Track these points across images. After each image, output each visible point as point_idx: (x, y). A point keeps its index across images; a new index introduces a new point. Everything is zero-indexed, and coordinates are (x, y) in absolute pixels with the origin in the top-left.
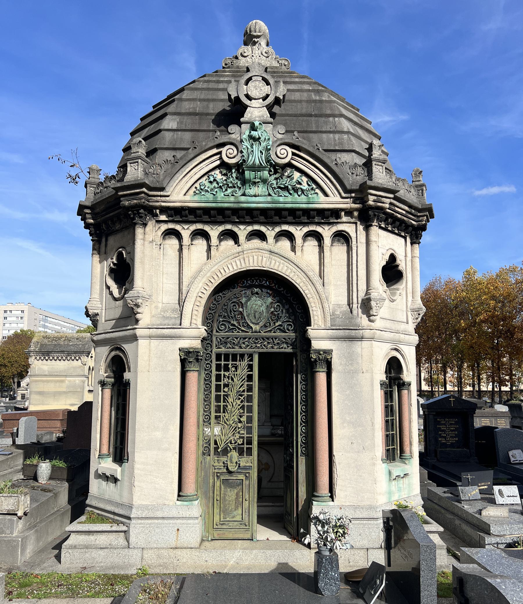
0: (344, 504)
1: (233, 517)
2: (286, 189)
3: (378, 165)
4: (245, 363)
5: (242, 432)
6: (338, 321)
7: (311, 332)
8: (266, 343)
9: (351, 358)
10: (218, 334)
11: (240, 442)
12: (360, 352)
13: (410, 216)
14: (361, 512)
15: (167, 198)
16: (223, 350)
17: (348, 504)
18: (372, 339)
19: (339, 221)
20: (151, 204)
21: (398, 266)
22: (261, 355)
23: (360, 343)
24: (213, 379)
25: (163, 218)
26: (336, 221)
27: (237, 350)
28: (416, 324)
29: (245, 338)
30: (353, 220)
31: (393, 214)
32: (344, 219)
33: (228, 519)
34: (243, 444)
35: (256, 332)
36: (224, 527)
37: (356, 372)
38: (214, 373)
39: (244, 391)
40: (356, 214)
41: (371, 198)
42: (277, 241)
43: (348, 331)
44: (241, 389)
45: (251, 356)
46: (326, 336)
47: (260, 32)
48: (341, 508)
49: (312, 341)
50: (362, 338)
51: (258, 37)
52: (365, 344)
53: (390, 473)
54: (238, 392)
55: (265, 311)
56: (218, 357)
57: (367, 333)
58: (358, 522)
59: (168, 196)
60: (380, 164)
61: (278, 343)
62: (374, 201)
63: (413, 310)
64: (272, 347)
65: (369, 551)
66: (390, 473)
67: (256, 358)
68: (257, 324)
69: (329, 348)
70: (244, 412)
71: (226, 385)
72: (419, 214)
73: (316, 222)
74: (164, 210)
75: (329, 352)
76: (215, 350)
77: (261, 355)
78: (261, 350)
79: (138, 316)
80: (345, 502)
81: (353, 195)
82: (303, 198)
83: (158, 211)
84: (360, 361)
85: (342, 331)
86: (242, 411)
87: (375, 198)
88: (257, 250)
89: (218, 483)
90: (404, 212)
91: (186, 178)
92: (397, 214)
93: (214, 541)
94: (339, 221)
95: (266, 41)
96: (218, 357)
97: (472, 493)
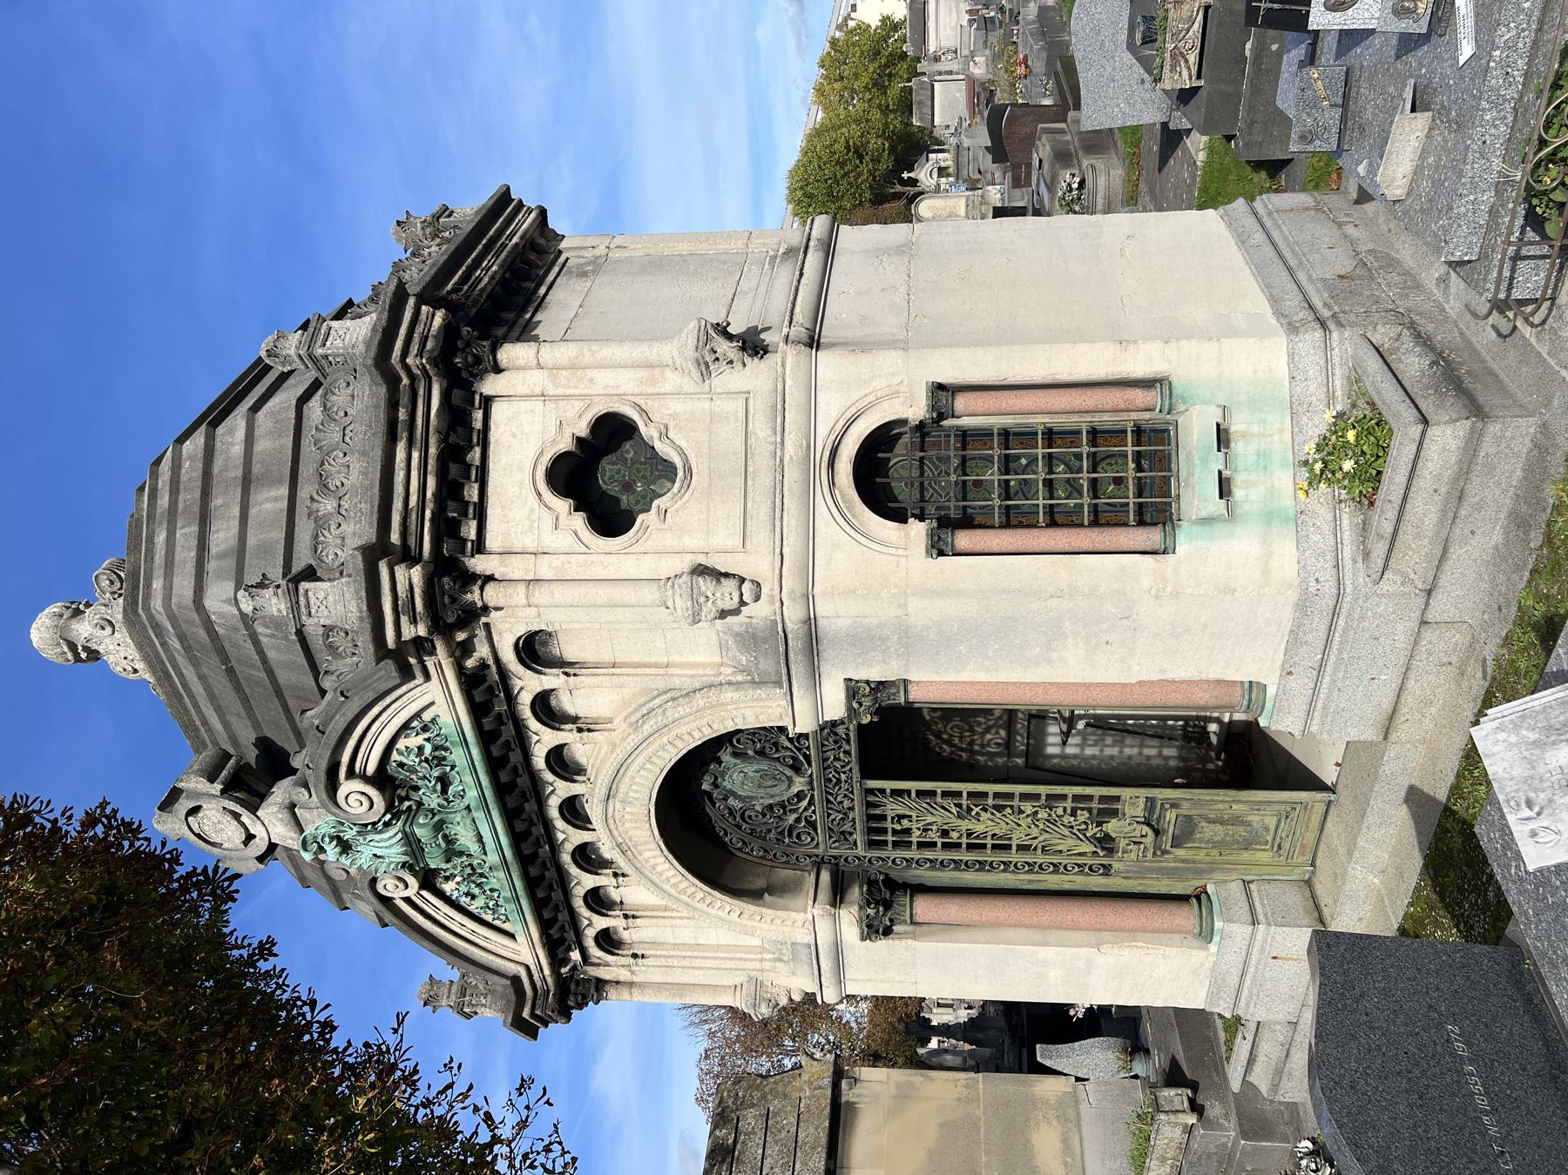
0: (1279, 663)
1: (1268, 830)
2: (444, 781)
3: (308, 605)
4: (892, 808)
5: (1060, 811)
6: (768, 665)
7: (805, 724)
8: (837, 764)
9: (864, 640)
10: (822, 846)
11: (1083, 816)
12: (849, 622)
13: (419, 421)
14: (1311, 631)
15: (533, 967)
16: (859, 837)
17: (1280, 656)
18: (808, 598)
19: (491, 662)
20: (552, 988)
21: (580, 441)
22: (865, 774)
23: (821, 622)
24: (929, 854)
25: (575, 955)
26: (494, 668)
27: (857, 814)
28: (748, 360)
29: (828, 801)
30: (481, 633)
31: (432, 520)
32: (482, 651)
33: (1269, 838)
34: (1090, 810)
35: (811, 782)
36: (1286, 845)
37: (906, 632)
38: (913, 854)
39: (959, 806)
40: (461, 636)
41: (408, 632)
42: (581, 770)
43: (791, 655)
44: (954, 810)
45: (870, 791)
46: (811, 698)
47: (59, 644)
48: (1290, 673)
49: (827, 718)
50: (810, 623)
51: (72, 646)
52: (823, 608)
53: (1207, 521)
54: (960, 816)
55: (756, 767)
56: (872, 844)
57: (793, 615)
58: (1337, 638)
59: (528, 968)
60: (302, 600)
61: (836, 742)
62: (414, 621)
63: (705, 369)
64: (847, 753)
65: (1430, 617)
66: (1207, 521)
67: (872, 784)
68: (790, 779)
69: (842, 685)
70: (1012, 807)
71: (945, 833)
72: (405, 381)
73: (509, 705)
74: (557, 961)
75: (852, 690)
76: (860, 851)
77: (865, 774)
78: (856, 774)
79: (797, 998)
80: (1273, 661)
81: (412, 661)
82: (457, 756)
83: (563, 970)
84: (875, 621)
85: (792, 667)
86: (1008, 810)
87: (404, 619)
88: (611, 821)
89: (1180, 852)
90: (415, 455)
91: (482, 943)
92: (429, 494)
93: (1318, 862)
94: (491, 662)
95: (74, 621)
96: (872, 844)
97: (1322, 93)
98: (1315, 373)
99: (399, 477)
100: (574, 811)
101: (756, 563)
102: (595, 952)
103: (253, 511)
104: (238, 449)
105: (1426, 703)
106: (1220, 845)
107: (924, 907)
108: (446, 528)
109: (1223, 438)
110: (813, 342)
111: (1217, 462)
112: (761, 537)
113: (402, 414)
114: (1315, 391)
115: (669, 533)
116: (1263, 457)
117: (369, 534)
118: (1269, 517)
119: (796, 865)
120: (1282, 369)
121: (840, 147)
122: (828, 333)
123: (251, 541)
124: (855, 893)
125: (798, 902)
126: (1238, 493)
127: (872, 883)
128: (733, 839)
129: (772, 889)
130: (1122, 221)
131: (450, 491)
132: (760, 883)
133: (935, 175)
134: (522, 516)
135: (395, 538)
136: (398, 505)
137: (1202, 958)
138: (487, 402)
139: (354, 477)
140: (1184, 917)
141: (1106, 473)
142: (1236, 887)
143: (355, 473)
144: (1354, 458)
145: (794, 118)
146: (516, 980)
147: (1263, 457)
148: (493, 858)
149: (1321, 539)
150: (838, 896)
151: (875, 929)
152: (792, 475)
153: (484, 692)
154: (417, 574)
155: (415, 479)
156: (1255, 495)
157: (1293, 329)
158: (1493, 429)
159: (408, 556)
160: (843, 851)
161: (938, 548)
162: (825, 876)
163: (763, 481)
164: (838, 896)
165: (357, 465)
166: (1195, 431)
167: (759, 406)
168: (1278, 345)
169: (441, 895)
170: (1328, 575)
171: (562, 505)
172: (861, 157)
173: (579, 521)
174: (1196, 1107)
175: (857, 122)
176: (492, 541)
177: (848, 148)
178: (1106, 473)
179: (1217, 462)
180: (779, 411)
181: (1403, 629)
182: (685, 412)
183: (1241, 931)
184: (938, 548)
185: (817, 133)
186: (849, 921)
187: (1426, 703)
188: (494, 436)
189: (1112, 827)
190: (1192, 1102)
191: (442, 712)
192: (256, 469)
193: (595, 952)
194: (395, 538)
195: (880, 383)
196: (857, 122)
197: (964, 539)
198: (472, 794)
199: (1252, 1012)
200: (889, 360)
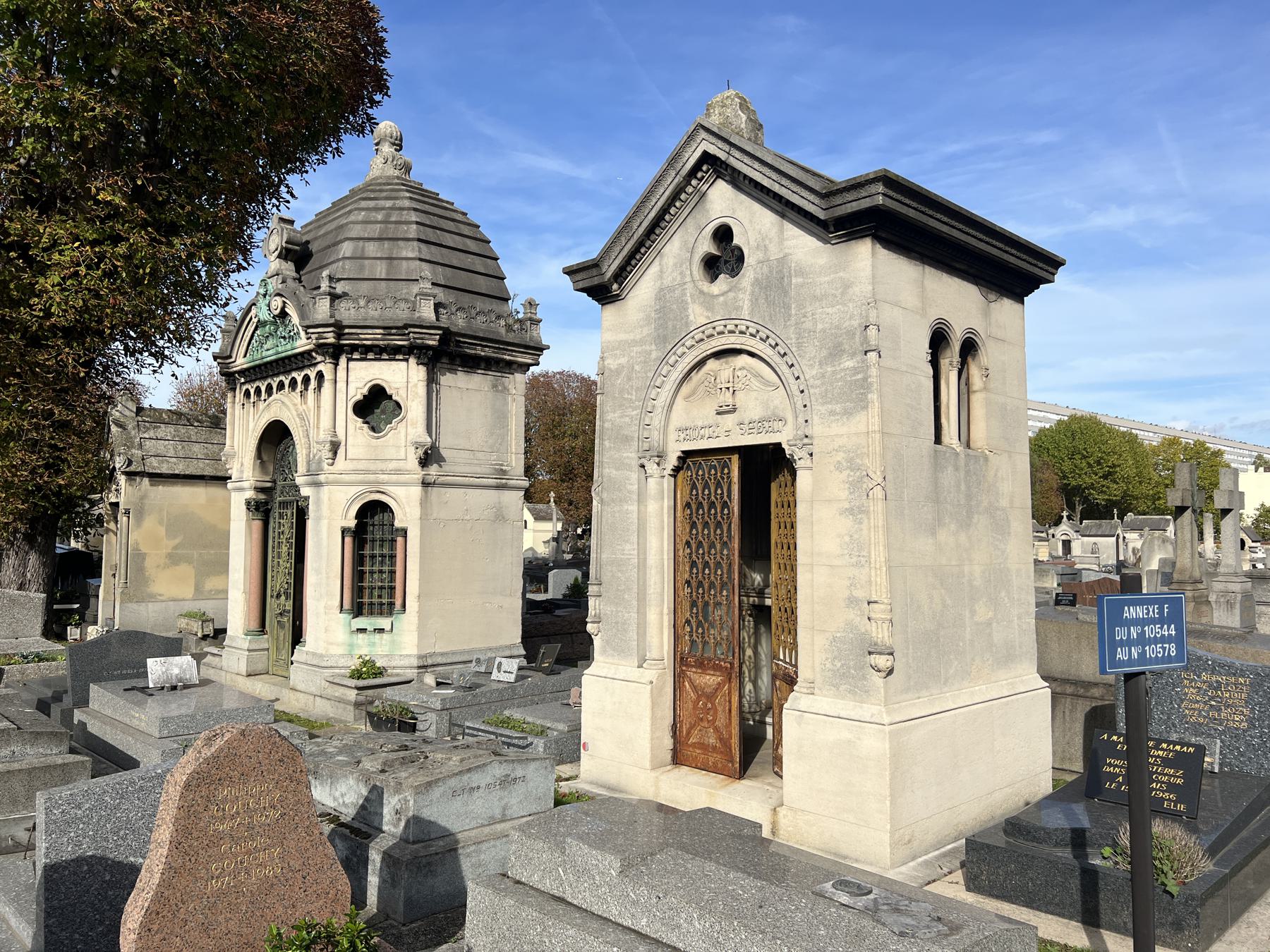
18: (328, 483)
52: (326, 488)
74: (242, 372)
75: (307, 498)
98: (402, 663)
99: (370, 331)
100: (281, 386)
101: (340, 462)
102: (244, 388)
103: (378, 262)
104: (404, 254)
105: (297, 700)
106: (278, 639)
107: (257, 524)
108: (354, 348)
109: (381, 630)
110: (425, 484)
111: (370, 628)
112: (350, 465)
113: (394, 331)
114: (394, 664)
115: (355, 432)
116: (374, 644)
117: (345, 323)
118: (351, 645)
119: (274, 473)
120: (404, 653)
121: (1113, 459)
122: (434, 491)
123: (367, 262)
124: (262, 497)
125: (257, 473)
126: (361, 635)
127: (266, 503)
128: (282, 447)
129: (263, 464)
130: (518, 604)
131: (368, 349)
132: (265, 458)
133: (1064, 537)
134: (362, 375)
135: (347, 331)
136: (359, 331)
137: (240, 633)
138: (407, 360)
139: (372, 313)
140: (254, 625)
141: (371, 591)
142: (266, 646)
143: (373, 313)
144: (368, 673)
145: (1153, 417)
146: (230, 357)
147: (374, 644)
148: (264, 354)
149: (342, 662)
150: (259, 490)
151: (248, 503)
152: (372, 477)
153: (303, 360)
154: (332, 340)
155: (370, 337)
156: (360, 641)
157: (420, 657)
158: (352, 708)
159: (339, 336)
160: (278, 492)
161: (344, 531)
162: (269, 485)
163: (372, 466)
164: (259, 490)
165: (376, 314)
166: (384, 622)
167: (401, 464)
168: (415, 652)
169: (256, 329)
170: (329, 664)
171: (365, 391)
172: (1105, 477)
173: (359, 397)
174: (205, 637)
175: (1139, 474)
176: (352, 364)
177: (1114, 466)
178: (371, 591)
179: (370, 628)
180: (398, 472)
181: (313, 690)
182: (408, 432)
183: (246, 646)
184: (344, 531)
185: (1131, 440)
186: (250, 494)
187: (297, 700)
188: (393, 363)
189: (283, 598)
190: (208, 636)
191: (298, 343)
192: (395, 262)
193: (244, 388)
194: (347, 331)
195: (408, 510)
196: (1139, 474)
197: (348, 540)
198: (280, 349)
199: (224, 653)
200: (416, 512)
